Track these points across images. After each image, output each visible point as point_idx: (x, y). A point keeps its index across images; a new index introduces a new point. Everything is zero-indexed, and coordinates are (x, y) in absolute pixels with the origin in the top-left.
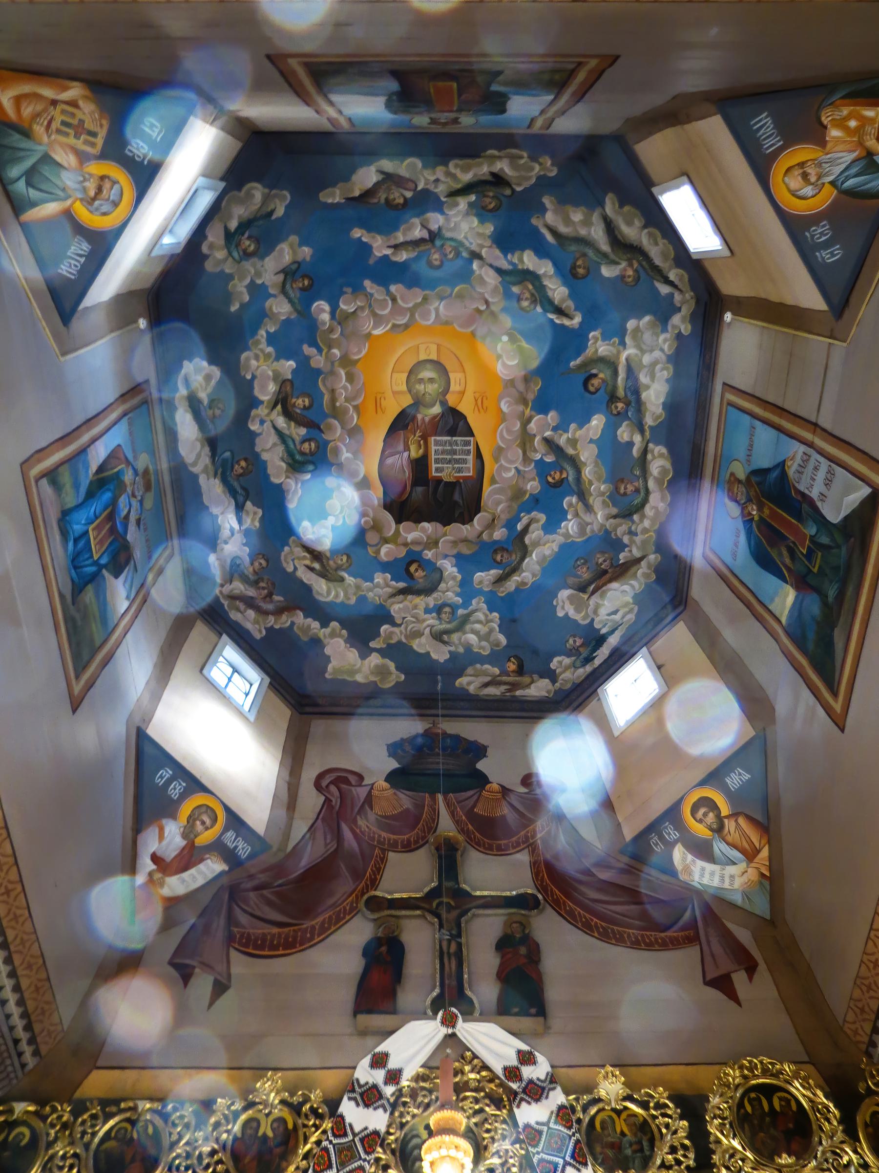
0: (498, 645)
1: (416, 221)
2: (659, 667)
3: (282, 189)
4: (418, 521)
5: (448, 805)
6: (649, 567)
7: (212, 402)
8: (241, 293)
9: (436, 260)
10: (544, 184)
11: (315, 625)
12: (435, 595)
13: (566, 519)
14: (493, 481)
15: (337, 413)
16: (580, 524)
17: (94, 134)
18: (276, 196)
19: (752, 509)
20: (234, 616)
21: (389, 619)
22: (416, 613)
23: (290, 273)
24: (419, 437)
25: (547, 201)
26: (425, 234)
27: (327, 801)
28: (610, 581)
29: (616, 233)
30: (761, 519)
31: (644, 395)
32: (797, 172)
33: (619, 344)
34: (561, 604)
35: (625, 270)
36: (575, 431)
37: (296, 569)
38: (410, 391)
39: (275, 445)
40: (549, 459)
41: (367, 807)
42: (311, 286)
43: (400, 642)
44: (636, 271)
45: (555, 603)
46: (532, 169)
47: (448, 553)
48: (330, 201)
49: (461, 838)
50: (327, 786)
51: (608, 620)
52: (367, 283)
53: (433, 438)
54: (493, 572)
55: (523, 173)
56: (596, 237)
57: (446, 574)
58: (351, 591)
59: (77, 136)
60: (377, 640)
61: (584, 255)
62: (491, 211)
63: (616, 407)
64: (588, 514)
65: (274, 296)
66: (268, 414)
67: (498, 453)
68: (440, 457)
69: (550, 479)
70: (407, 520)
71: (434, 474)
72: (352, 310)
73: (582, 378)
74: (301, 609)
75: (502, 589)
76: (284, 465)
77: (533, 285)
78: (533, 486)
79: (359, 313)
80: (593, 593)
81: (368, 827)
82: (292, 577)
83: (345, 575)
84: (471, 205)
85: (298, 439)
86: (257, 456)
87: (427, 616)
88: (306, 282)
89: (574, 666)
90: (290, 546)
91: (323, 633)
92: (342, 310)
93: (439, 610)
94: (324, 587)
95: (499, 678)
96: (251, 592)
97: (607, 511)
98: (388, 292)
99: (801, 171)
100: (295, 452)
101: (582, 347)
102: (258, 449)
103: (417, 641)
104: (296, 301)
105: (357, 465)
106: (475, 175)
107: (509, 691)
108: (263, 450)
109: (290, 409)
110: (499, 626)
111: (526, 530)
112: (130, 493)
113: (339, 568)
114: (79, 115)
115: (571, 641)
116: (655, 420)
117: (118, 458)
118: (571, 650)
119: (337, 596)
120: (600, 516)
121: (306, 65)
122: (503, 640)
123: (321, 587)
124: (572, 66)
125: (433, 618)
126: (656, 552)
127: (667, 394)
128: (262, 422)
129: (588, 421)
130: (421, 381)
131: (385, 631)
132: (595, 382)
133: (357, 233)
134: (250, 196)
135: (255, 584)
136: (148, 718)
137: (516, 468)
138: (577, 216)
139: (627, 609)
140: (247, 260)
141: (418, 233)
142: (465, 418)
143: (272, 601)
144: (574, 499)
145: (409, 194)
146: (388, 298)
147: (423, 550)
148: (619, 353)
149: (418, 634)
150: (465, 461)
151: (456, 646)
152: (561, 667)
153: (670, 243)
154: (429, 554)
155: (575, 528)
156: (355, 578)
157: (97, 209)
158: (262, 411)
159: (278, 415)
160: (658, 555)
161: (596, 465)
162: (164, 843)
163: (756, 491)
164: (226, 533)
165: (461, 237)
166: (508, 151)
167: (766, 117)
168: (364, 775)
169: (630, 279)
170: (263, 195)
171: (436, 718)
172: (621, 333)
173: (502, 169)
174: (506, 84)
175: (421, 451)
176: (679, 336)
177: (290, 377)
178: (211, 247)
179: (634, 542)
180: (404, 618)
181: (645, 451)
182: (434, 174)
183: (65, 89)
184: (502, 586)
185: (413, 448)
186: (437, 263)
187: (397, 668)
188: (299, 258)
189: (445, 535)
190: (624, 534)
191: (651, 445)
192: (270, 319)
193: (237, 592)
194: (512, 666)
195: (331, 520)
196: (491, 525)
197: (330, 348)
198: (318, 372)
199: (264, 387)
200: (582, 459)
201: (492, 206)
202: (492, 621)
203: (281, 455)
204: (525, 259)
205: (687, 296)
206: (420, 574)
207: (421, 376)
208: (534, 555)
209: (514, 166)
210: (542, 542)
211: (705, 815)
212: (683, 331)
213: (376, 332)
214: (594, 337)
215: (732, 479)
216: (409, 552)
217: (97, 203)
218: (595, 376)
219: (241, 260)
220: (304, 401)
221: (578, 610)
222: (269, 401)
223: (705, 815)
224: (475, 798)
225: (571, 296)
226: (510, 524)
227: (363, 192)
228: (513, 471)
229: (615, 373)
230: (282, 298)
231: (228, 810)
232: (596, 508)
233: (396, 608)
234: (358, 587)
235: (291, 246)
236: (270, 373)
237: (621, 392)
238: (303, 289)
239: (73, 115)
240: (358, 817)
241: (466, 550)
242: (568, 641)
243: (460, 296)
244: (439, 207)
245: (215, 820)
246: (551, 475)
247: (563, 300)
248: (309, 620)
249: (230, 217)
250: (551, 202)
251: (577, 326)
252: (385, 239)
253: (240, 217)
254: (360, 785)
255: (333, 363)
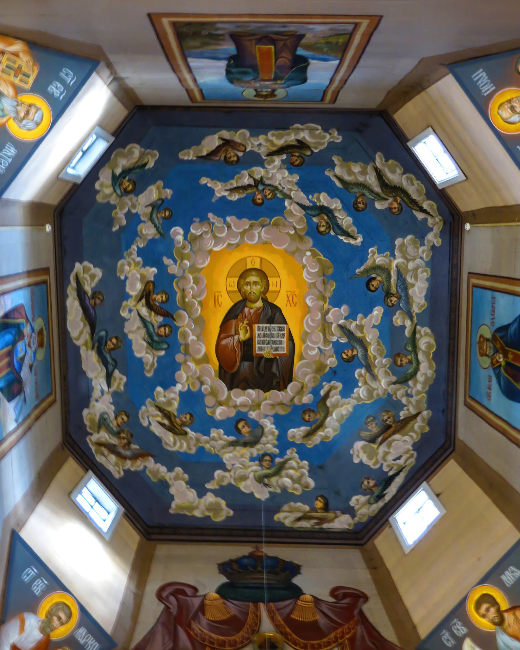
0: (307, 487)
1: (245, 172)
2: (438, 495)
3: (153, 150)
4: (244, 389)
5: (269, 612)
6: (423, 420)
7: (95, 294)
8: (121, 219)
9: (259, 199)
10: (332, 147)
11: (163, 469)
12: (258, 446)
13: (358, 386)
14: (301, 358)
15: (186, 307)
16: (369, 389)
17: (28, 76)
18: (148, 153)
19: (500, 358)
20: (100, 459)
21: (222, 466)
22: (244, 461)
23: (155, 207)
24: (247, 324)
25: (335, 159)
26: (252, 182)
27: (167, 608)
28: (394, 433)
29: (384, 178)
30: (508, 364)
31: (410, 292)
32: (507, 106)
33: (390, 256)
34: (356, 453)
35: (392, 204)
36: (361, 319)
37: (150, 424)
38: (239, 290)
39: (139, 328)
40: (344, 340)
41: (200, 614)
42: (171, 216)
43: (230, 485)
44: (399, 204)
45: (351, 452)
46: (325, 137)
47: (268, 414)
48: (186, 158)
49: (279, 636)
50: (167, 597)
51: (393, 464)
52: (210, 215)
53: (256, 325)
54: (303, 428)
55: (319, 140)
56: (370, 182)
57: (266, 430)
58: (193, 442)
59: (16, 76)
60: (212, 482)
61: (363, 195)
62: (297, 166)
63: (391, 301)
64: (374, 382)
65: (144, 222)
66: (135, 306)
67: (305, 336)
68: (262, 339)
69: (344, 356)
70: (237, 387)
71: (257, 352)
72: (200, 233)
73: (365, 279)
74: (152, 456)
75: (310, 442)
76: (145, 344)
77: (327, 216)
78: (331, 361)
79: (204, 236)
80: (381, 443)
81: (200, 629)
82: (147, 430)
83: (188, 430)
84: (283, 161)
85: (156, 325)
86: (125, 335)
87: (252, 463)
88: (167, 213)
89: (369, 503)
90: (146, 406)
91: (169, 476)
92: (192, 234)
93: (260, 459)
94: (172, 439)
95: (309, 514)
96: (114, 441)
97: (388, 380)
98: (225, 222)
99: (509, 105)
100: (154, 334)
101: (364, 259)
102: (126, 331)
103: (243, 483)
104: (160, 226)
105: (201, 346)
106: (286, 141)
107: (317, 524)
108: (130, 332)
109: (151, 302)
110: (309, 472)
111: (327, 395)
112: (27, 343)
113: (184, 424)
114: (19, 62)
115: (365, 483)
116: (419, 309)
117: (21, 314)
118: (365, 490)
119: (181, 446)
120: (383, 383)
121: (174, 25)
122: (312, 483)
123: (169, 440)
124: (350, 28)
125: (256, 465)
126: (427, 409)
127: (428, 289)
128: (130, 311)
129: (371, 312)
130: (248, 283)
131: (218, 475)
132: (375, 283)
133: (204, 181)
134: (131, 152)
135: (117, 434)
136: (22, 524)
137: (319, 348)
138: (356, 168)
139: (408, 455)
140: (127, 196)
141: (246, 181)
142: (280, 310)
143: (130, 449)
144: (363, 371)
145: (240, 154)
146: (225, 226)
147: (249, 411)
148: (391, 261)
149: (244, 478)
150: (280, 342)
151: (275, 488)
152: (358, 504)
153: (422, 183)
154: (253, 415)
155: (365, 393)
156: (195, 432)
157: (24, 126)
158: (131, 303)
159: (143, 306)
160: (429, 411)
161: (379, 344)
162: (25, 634)
163: (500, 343)
164: (96, 394)
165: (276, 184)
166: (308, 125)
167: (482, 72)
168: (196, 586)
169: (396, 210)
170: (140, 152)
171: (260, 544)
172: (392, 249)
173: (304, 137)
174: (307, 47)
175: (248, 335)
176: (433, 247)
177: (152, 279)
178: (102, 185)
179: (411, 402)
180: (233, 465)
181: (414, 332)
182: (258, 140)
183: (10, 44)
184: (310, 440)
185: (242, 332)
186: (260, 201)
187: (228, 506)
188: (163, 197)
189: (265, 399)
190: (403, 396)
191: (418, 327)
192: (140, 238)
193: (103, 440)
194: (319, 504)
195: (179, 387)
196: (300, 391)
197: (182, 259)
198: (173, 277)
199: (133, 287)
200: (368, 340)
201: (298, 162)
202: (302, 467)
203: (143, 336)
204: (321, 198)
205: (437, 220)
206: (245, 430)
207: (248, 280)
208: (334, 415)
209: (312, 136)
210: (340, 404)
211: (488, 610)
212: (436, 244)
213: (216, 249)
214: (372, 252)
215: (482, 339)
216: (239, 413)
217: (24, 122)
218: (374, 279)
219: (122, 196)
220: (162, 297)
221: (370, 458)
222: (136, 296)
223: (488, 610)
224: (291, 607)
225: (354, 223)
226: (315, 391)
227: (209, 152)
228: (317, 349)
229: (389, 276)
230: (149, 223)
231: (82, 609)
232: (380, 377)
233: (227, 457)
234: (198, 440)
235: (158, 188)
236: (139, 276)
237: (394, 290)
238: (165, 218)
239: (14, 62)
240: (193, 622)
241: (282, 412)
242: (363, 483)
243: (276, 225)
244: (261, 163)
245: (69, 616)
246: (344, 353)
247: (349, 226)
248: (159, 465)
249: (116, 166)
250: (339, 160)
251: (360, 245)
252: (223, 184)
253: (123, 166)
254: (194, 596)
255: (184, 271)
